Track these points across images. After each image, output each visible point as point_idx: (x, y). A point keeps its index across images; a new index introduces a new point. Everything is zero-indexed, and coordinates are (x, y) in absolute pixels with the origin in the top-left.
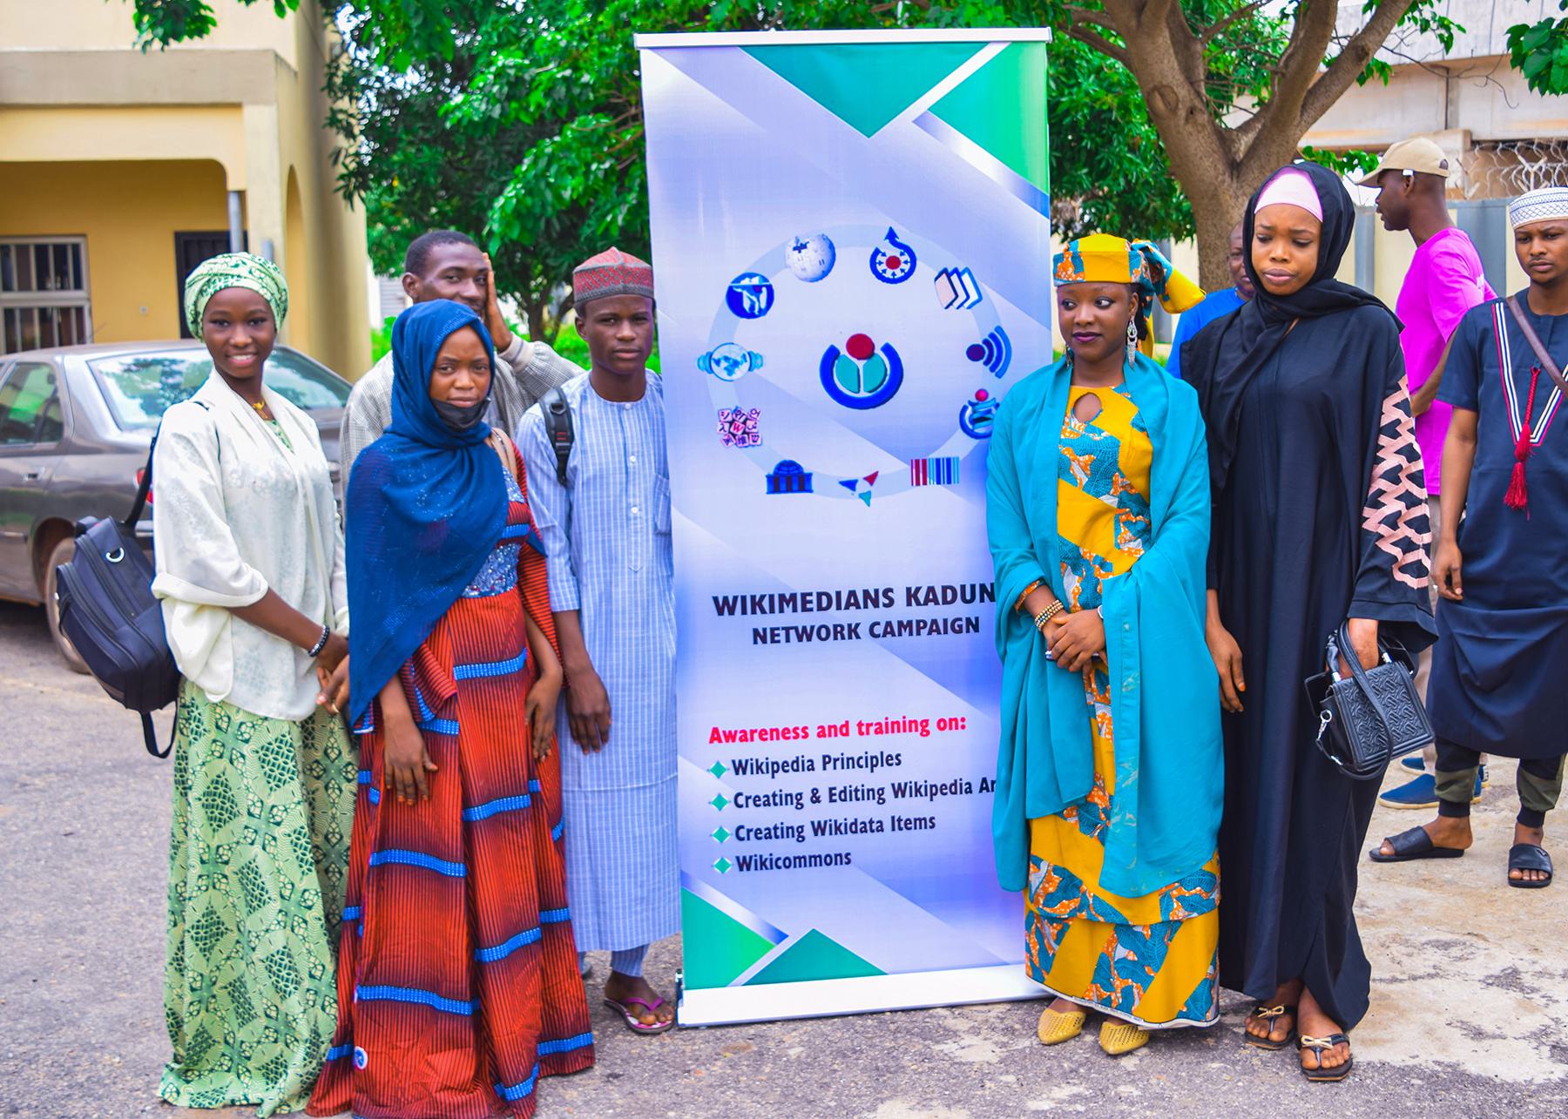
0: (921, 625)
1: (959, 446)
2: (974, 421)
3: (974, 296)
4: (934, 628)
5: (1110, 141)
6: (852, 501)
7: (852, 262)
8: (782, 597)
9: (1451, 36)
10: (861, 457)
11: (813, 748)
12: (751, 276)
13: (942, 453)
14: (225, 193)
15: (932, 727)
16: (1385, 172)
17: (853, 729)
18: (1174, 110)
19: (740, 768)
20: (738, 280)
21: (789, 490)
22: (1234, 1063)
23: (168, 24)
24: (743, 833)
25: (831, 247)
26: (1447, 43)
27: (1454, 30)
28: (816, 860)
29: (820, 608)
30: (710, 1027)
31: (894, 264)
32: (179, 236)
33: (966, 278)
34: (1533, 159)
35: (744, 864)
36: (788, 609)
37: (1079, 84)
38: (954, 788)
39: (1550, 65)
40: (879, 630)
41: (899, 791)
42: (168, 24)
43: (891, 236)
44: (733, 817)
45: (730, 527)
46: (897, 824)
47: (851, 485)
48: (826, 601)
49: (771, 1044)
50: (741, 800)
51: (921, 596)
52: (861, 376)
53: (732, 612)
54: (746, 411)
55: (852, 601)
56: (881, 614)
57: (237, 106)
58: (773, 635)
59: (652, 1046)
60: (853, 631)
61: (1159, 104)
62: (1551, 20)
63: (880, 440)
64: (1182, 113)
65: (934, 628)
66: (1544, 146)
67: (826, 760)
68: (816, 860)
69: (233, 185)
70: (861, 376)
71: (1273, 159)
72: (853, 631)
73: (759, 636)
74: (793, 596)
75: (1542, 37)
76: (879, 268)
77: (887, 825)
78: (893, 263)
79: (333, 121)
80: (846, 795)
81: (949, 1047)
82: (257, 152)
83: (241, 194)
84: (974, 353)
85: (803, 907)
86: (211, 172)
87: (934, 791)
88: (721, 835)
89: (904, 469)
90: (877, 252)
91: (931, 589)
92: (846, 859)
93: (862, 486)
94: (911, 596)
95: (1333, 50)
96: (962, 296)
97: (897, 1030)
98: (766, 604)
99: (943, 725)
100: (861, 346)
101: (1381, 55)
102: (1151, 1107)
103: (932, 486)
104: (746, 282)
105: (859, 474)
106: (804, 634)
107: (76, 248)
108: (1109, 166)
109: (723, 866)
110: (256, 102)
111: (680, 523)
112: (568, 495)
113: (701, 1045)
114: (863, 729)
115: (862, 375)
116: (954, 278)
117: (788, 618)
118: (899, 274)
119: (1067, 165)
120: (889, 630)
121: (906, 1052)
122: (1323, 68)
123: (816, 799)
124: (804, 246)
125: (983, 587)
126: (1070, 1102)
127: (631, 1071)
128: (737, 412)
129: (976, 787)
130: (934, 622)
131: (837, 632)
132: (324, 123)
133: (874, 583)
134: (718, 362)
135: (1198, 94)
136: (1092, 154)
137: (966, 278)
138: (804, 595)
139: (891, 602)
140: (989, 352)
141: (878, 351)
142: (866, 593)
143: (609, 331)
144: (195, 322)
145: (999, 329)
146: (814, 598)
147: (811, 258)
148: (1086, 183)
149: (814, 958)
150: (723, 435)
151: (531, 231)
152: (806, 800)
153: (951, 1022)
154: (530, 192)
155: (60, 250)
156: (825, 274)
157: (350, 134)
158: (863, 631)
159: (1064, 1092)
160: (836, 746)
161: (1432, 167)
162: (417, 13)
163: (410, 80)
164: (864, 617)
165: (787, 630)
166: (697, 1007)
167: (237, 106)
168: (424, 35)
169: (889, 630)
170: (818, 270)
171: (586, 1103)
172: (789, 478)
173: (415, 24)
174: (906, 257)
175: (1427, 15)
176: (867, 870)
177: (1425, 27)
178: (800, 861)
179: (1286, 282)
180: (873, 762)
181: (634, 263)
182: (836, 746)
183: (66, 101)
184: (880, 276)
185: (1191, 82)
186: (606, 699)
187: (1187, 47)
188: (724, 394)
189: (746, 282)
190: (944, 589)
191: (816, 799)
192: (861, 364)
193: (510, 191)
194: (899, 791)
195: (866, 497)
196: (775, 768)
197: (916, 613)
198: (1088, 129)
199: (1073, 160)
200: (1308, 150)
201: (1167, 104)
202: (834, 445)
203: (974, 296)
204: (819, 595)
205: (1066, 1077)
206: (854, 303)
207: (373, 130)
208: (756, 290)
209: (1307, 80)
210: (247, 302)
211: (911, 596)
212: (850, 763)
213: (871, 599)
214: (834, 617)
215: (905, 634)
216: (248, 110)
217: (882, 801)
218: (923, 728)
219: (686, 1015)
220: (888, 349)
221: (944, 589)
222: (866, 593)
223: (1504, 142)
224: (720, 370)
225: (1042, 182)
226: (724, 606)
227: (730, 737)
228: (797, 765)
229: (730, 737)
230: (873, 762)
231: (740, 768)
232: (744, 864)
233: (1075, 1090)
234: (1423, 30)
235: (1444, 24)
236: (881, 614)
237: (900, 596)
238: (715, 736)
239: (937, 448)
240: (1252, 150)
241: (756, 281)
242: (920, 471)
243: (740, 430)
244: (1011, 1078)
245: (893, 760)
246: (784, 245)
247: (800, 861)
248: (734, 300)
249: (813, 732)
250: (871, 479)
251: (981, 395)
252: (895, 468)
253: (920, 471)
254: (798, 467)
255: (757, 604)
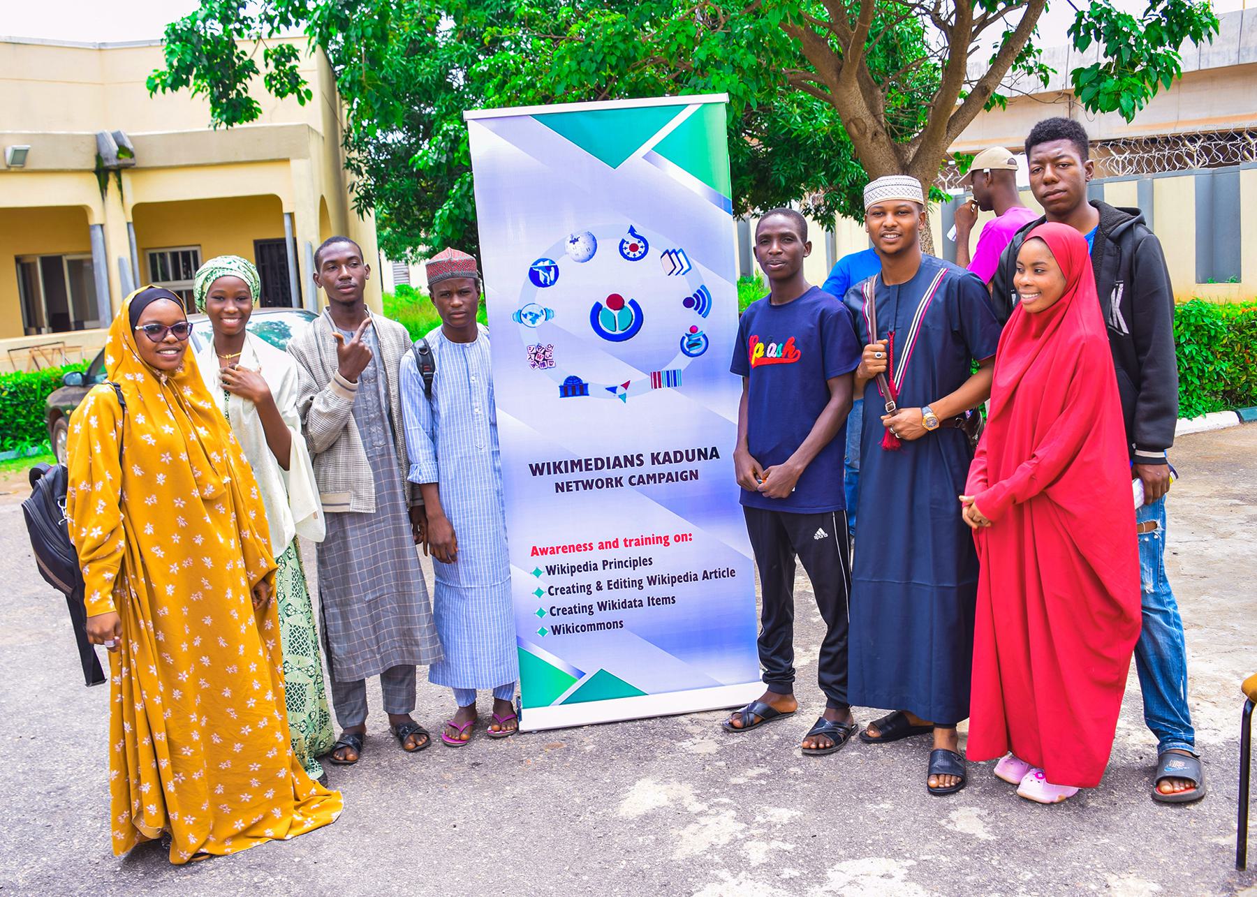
0: (661, 476)
1: (680, 362)
2: (689, 346)
3: (686, 267)
4: (670, 478)
5: (839, 154)
6: (614, 400)
7: (608, 249)
8: (572, 462)
9: (1047, 76)
10: (619, 372)
11: (596, 556)
12: (544, 260)
13: (670, 367)
14: (282, 215)
15: (671, 540)
16: (974, 172)
17: (621, 543)
18: (864, 134)
19: (551, 570)
20: (536, 263)
21: (574, 395)
22: (866, 752)
23: (230, 113)
24: (554, 611)
25: (594, 239)
26: (1046, 81)
27: (1049, 72)
28: (600, 626)
29: (597, 468)
30: (539, 731)
31: (634, 249)
32: (256, 242)
33: (680, 255)
34: (1121, 152)
35: (556, 630)
36: (577, 470)
37: (816, 118)
38: (687, 578)
39: (1098, 93)
40: (634, 481)
41: (652, 581)
42: (230, 113)
43: (632, 231)
44: (547, 601)
45: (535, 420)
46: (651, 601)
47: (613, 390)
48: (600, 463)
49: (576, 743)
50: (553, 591)
51: (661, 458)
52: (616, 320)
53: (541, 473)
54: (544, 346)
55: (617, 463)
56: (636, 471)
57: (287, 160)
58: (568, 487)
59: (502, 745)
60: (619, 482)
61: (854, 130)
62: (1098, 64)
63: (630, 361)
64: (869, 135)
65: (670, 478)
66: (1126, 143)
67: (605, 563)
68: (600, 626)
69: (285, 210)
70: (616, 320)
71: (930, 162)
72: (619, 482)
73: (559, 487)
74: (580, 461)
75: (1093, 75)
76: (625, 252)
77: (645, 602)
78: (634, 248)
79: (349, 165)
80: (618, 585)
81: (686, 744)
82: (301, 188)
83: (291, 215)
84: (688, 303)
85: (593, 656)
86: (273, 202)
87: (674, 580)
88: (541, 613)
89: (647, 378)
90: (623, 241)
91: (667, 454)
92: (620, 624)
93: (620, 390)
94: (655, 458)
95: (967, 89)
96: (679, 267)
97: (655, 734)
98: (562, 467)
99: (677, 538)
100: (615, 301)
101: (1000, 91)
102: (808, 781)
103: (665, 389)
104: (541, 264)
105: (618, 383)
106: (588, 485)
107: (195, 253)
108: (838, 170)
109: (543, 632)
110: (299, 157)
111: (501, 415)
112: (431, 405)
113: (532, 743)
114: (628, 543)
115: (617, 320)
116: (673, 255)
117: (577, 475)
118: (638, 255)
119: (811, 171)
120: (641, 480)
121: (659, 747)
122: (960, 101)
123: (599, 588)
124: (576, 240)
125: (699, 450)
126: (758, 779)
127: (487, 761)
128: (539, 347)
129: (700, 577)
130: (670, 474)
131: (609, 482)
132: (339, 168)
133: (631, 451)
134: (525, 316)
135: (880, 122)
136: (827, 162)
137: (680, 255)
138: (586, 461)
139: (642, 463)
140: (698, 301)
141: (626, 304)
142: (626, 457)
143: (447, 302)
144: (201, 299)
145: (703, 287)
146: (593, 462)
147: (582, 248)
148: (824, 181)
149: (602, 686)
150: (530, 362)
151: (459, 231)
152: (593, 589)
153: (690, 728)
154: (458, 206)
155: (186, 255)
156: (591, 257)
157: (359, 173)
158: (625, 481)
159: (757, 771)
160: (610, 554)
161: (1003, 165)
162: (377, 100)
163: (397, 137)
164: (625, 472)
165: (577, 482)
166: (531, 719)
167: (287, 160)
168: (382, 113)
169: (641, 480)
170: (586, 254)
171: (457, 781)
172: (574, 387)
173: (376, 107)
174: (642, 244)
175: (1031, 64)
176: (632, 630)
177: (1030, 71)
178: (591, 627)
179: (779, 269)
180: (634, 563)
181: (459, 256)
182: (610, 554)
183: (183, 163)
184: (626, 257)
185: (875, 115)
186: (453, 534)
187: (872, 93)
188: (530, 336)
189: (541, 264)
190: (675, 453)
191: (599, 588)
192: (616, 313)
193: (446, 206)
194: (652, 581)
195: (623, 397)
196: (573, 570)
197: (658, 469)
198: (824, 147)
199: (814, 167)
200: (957, 155)
201: (859, 130)
202: (601, 365)
203: (686, 267)
204: (596, 460)
205: (757, 763)
206: (612, 275)
207: (374, 171)
208: (548, 269)
209: (949, 110)
210: (236, 285)
211: (655, 458)
212: (620, 564)
213: (629, 461)
214: (606, 473)
215: (652, 482)
216: (293, 163)
217: (641, 588)
218: (665, 541)
219: (523, 726)
220: (633, 303)
221: (675, 453)
222: (626, 457)
223: (1102, 141)
224: (527, 321)
225: (726, 190)
226: (536, 470)
227: (544, 551)
228: (586, 567)
229: (544, 551)
230: (634, 563)
231: (551, 570)
232: (556, 630)
233: (762, 771)
234: (1029, 73)
235: (1042, 69)
236: (636, 471)
237: (647, 459)
238: (535, 551)
239: (666, 364)
240: (916, 156)
241: (547, 264)
242: (657, 380)
243: (541, 358)
244: (723, 763)
245: (647, 562)
246: (564, 240)
247: (591, 627)
248: (534, 276)
249: (596, 546)
250: (626, 385)
251: (694, 329)
252: (640, 378)
253: (657, 380)
254: (579, 380)
255: (557, 467)
